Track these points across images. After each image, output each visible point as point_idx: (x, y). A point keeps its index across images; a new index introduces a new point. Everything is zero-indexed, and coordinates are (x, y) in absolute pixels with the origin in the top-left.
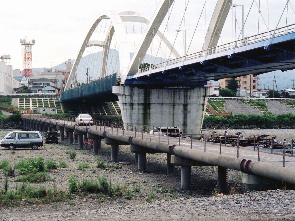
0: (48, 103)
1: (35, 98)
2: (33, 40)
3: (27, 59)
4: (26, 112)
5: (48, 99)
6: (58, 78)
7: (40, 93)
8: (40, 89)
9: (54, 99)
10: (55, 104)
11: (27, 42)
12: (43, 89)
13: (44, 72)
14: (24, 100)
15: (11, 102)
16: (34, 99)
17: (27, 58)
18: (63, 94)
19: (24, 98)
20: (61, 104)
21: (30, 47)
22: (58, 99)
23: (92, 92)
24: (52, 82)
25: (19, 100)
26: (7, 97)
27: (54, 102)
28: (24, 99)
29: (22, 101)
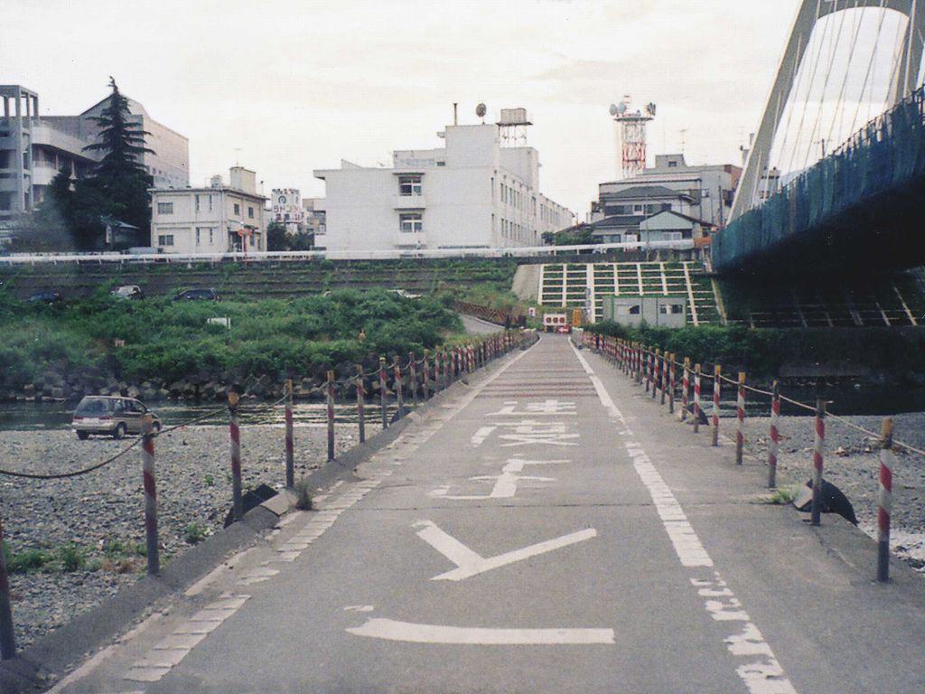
0: (660, 281)
1: (607, 264)
2: (648, 103)
3: (631, 164)
4: (562, 320)
5: (662, 264)
6: (706, 185)
7: (630, 243)
8: (632, 225)
9: (685, 263)
10: (689, 285)
11: (631, 110)
12: (643, 225)
13: (654, 167)
14: (565, 272)
15: (512, 282)
16: (603, 268)
17: (632, 161)
18: (720, 240)
19: (565, 265)
20: (713, 285)
21: (639, 127)
22: (699, 264)
23: (863, 186)
24: (681, 198)
25: (542, 272)
26: (495, 262)
27: (687, 276)
28: (565, 269)
29: (556, 275)
